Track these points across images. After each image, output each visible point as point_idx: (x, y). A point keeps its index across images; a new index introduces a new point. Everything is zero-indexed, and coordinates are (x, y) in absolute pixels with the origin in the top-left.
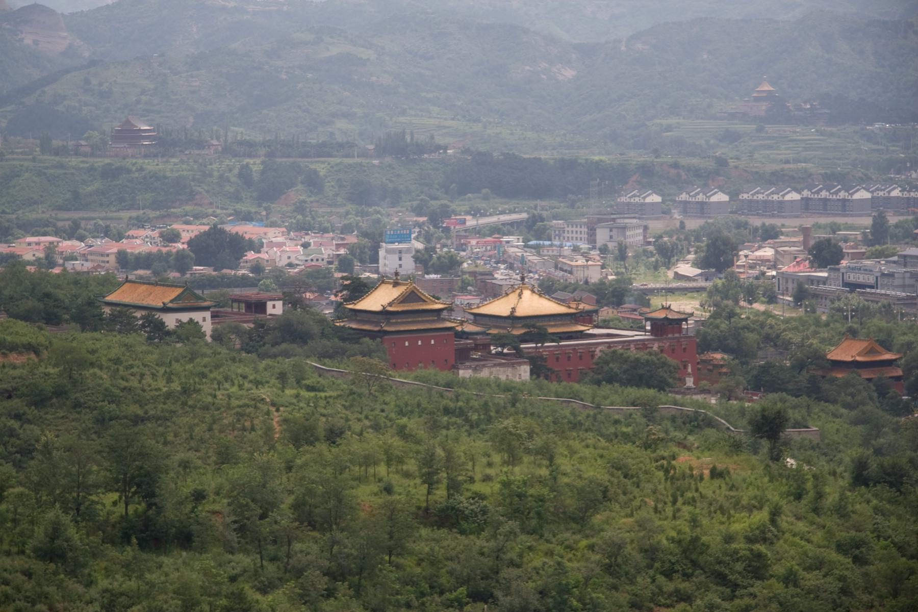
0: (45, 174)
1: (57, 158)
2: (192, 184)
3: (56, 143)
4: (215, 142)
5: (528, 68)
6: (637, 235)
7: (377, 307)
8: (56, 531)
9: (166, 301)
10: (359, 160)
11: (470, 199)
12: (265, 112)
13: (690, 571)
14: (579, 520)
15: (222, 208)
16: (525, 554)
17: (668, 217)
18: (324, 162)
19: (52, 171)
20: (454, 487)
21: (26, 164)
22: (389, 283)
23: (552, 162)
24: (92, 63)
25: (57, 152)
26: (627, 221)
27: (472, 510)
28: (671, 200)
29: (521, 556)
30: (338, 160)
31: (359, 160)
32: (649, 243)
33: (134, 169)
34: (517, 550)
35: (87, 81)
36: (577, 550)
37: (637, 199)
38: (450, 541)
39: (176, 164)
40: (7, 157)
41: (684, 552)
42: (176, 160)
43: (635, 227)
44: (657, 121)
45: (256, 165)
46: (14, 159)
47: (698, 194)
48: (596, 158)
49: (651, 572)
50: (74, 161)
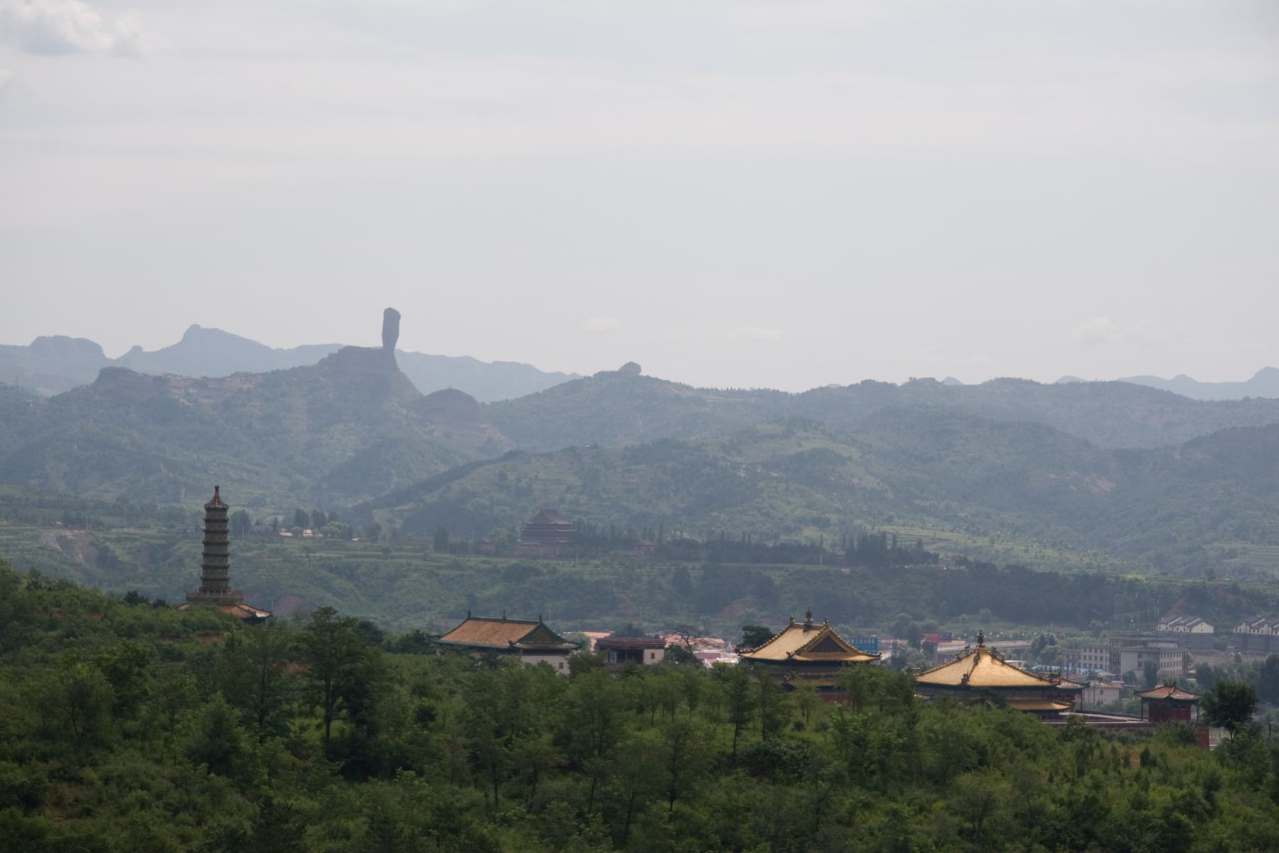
0: (437, 575)
1: (453, 557)
2: (615, 590)
3: (452, 539)
4: (647, 542)
5: (1053, 476)
6: (1175, 664)
7: (781, 656)
8: (218, 726)
9: (514, 640)
10: (825, 568)
11: (964, 621)
12: (715, 514)
13: (1082, 842)
14: (940, 780)
15: (650, 621)
16: (858, 812)
17: (1222, 653)
18: (781, 569)
19: (446, 572)
20: (772, 727)
21: (415, 562)
22: (798, 627)
23: (1072, 579)
24: (511, 455)
25: (453, 550)
26: (1161, 645)
27: (792, 756)
28: (1228, 634)
29: (851, 813)
30: (799, 567)
31: (825, 568)
32: (1191, 676)
33: (545, 571)
34: (847, 806)
35: (503, 476)
36: (930, 811)
37: (1181, 629)
38: (759, 792)
39: (597, 566)
40: (394, 554)
41: (1075, 817)
42: (597, 562)
43: (1171, 653)
44: (1216, 545)
45: (695, 570)
46: (400, 557)
47: (1262, 625)
48: (1130, 577)
49: (1027, 840)
50: (473, 560)
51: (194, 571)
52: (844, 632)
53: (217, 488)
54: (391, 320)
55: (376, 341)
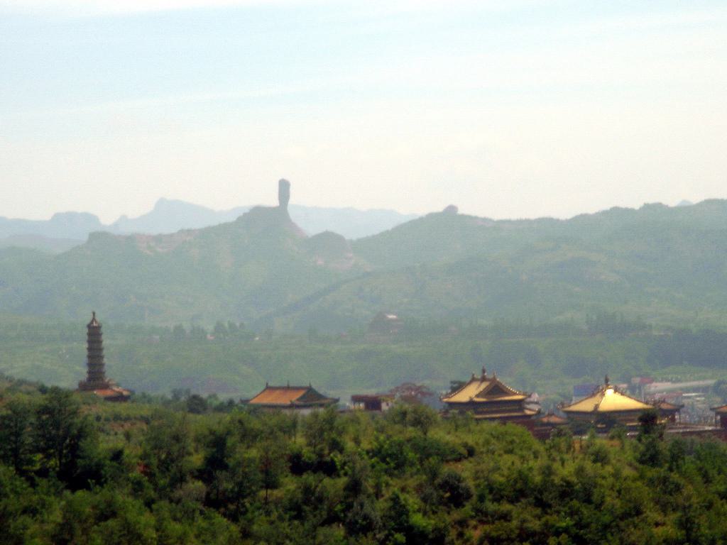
51: (82, 372)
52: (504, 381)
53: (94, 314)
54: (284, 187)
55: (274, 201)
